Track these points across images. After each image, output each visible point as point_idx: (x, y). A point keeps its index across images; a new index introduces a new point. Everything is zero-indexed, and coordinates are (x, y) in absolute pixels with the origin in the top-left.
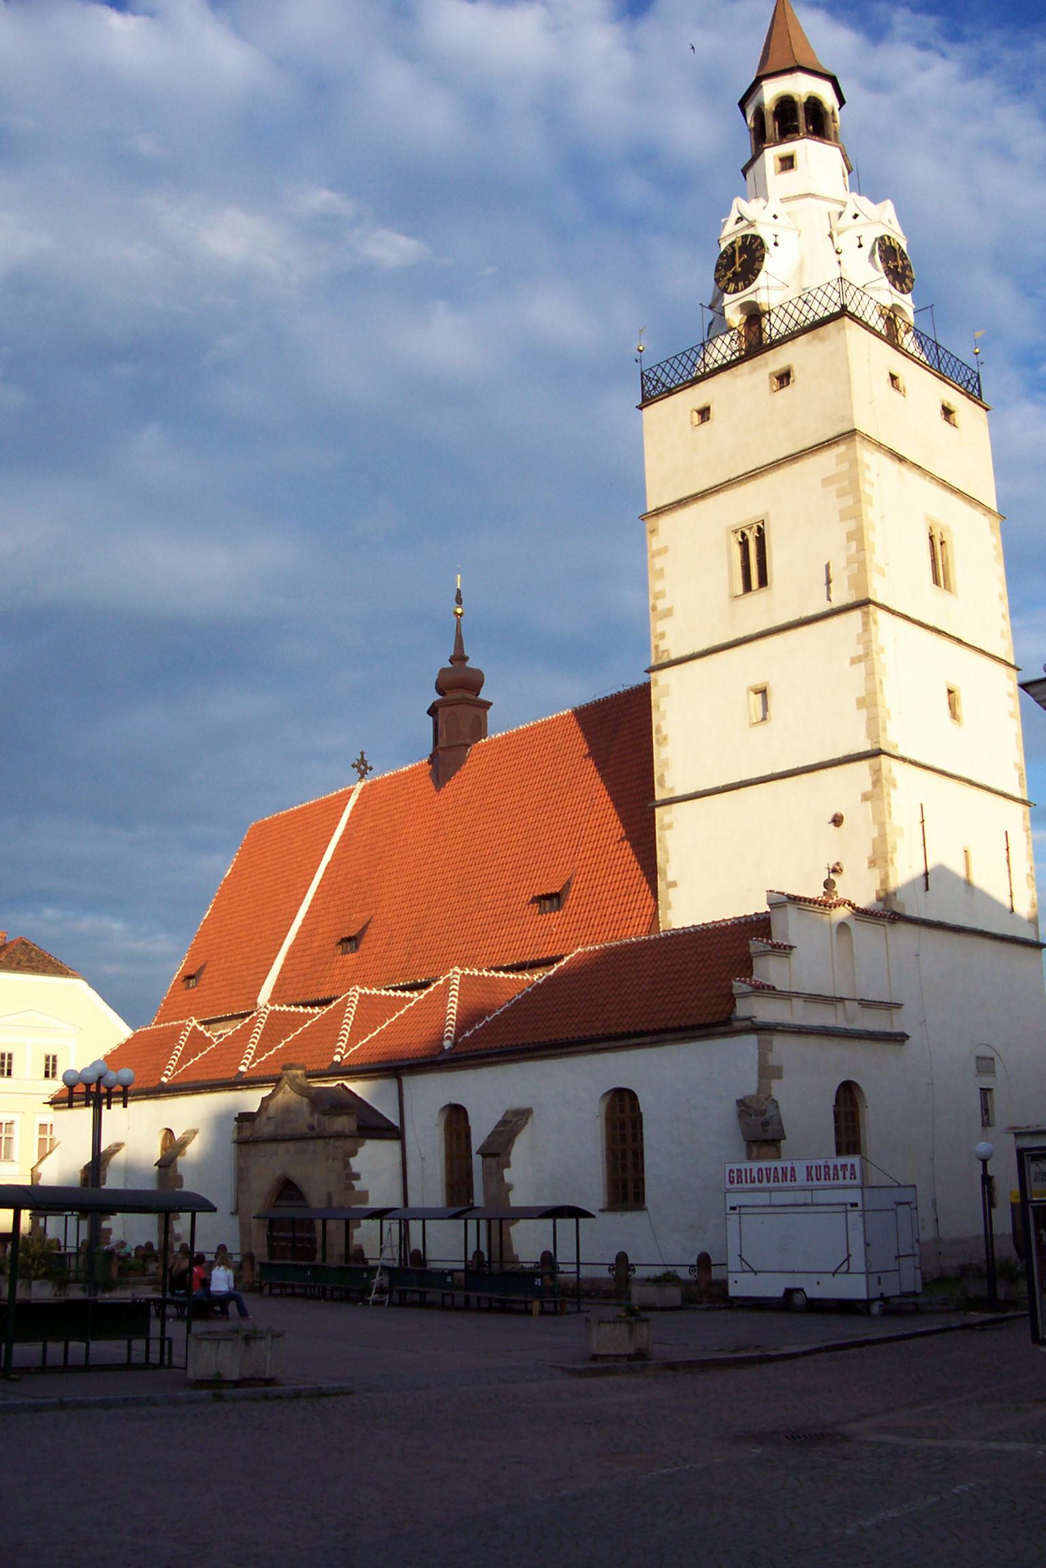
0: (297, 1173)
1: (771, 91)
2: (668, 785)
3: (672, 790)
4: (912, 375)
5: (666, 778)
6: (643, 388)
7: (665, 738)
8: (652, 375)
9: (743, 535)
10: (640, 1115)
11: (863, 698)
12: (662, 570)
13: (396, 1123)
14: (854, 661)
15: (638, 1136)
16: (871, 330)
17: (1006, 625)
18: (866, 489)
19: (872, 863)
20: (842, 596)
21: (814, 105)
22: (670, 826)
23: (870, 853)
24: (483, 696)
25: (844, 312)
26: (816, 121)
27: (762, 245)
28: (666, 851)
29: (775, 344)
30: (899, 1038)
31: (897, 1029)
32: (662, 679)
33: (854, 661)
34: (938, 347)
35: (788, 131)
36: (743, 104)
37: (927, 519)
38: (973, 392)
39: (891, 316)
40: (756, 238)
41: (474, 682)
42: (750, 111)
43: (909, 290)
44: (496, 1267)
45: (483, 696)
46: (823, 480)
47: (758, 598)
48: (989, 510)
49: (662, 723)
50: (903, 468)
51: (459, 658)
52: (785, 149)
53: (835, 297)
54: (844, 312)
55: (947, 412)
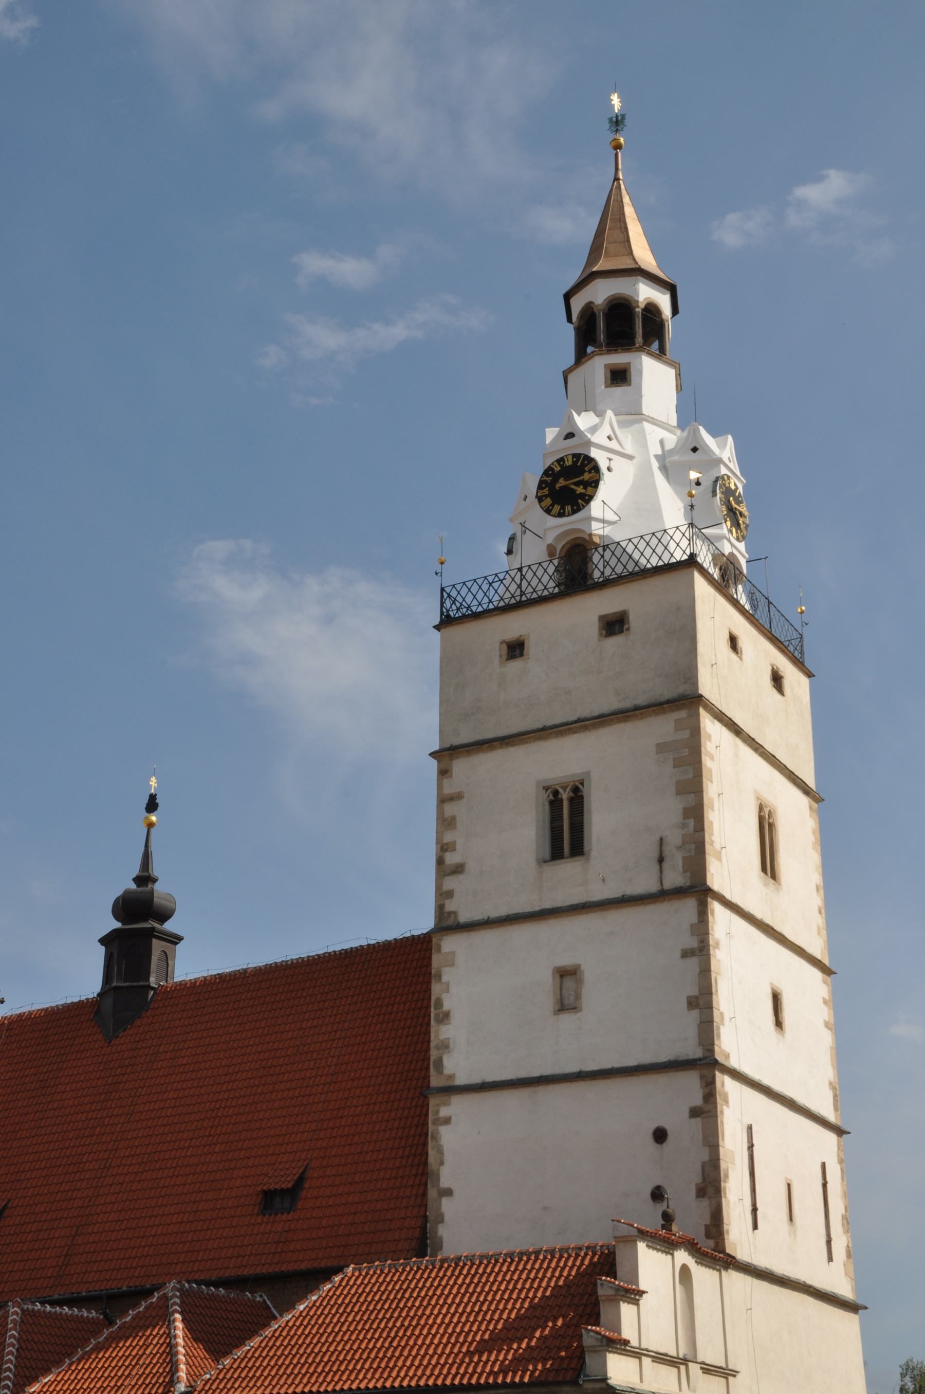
1: (600, 293)
2: (447, 1071)
3: (452, 1077)
4: (748, 635)
6: (442, 606)
7: (447, 1015)
8: (454, 594)
9: (556, 793)
11: (696, 998)
12: (454, 818)
14: (685, 954)
17: (819, 920)
18: (707, 762)
19: (701, 1192)
20: (675, 878)
22: (447, 1121)
23: (698, 1179)
24: (169, 926)
25: (692, 562)
28: (440, 1151)
29: (607, 583)
32: (449, 944)
34: (770, 603)
36: (568, 297)
37: (758, 799)
38: (799, 663)
42: (578, 304)
43: (744, 538)
46: (658, 745)
47: (568, 868)
49: (444, 997)
51: (144, 879)
52: (618, 359)
54: (692, 562)
55: (733, 642)
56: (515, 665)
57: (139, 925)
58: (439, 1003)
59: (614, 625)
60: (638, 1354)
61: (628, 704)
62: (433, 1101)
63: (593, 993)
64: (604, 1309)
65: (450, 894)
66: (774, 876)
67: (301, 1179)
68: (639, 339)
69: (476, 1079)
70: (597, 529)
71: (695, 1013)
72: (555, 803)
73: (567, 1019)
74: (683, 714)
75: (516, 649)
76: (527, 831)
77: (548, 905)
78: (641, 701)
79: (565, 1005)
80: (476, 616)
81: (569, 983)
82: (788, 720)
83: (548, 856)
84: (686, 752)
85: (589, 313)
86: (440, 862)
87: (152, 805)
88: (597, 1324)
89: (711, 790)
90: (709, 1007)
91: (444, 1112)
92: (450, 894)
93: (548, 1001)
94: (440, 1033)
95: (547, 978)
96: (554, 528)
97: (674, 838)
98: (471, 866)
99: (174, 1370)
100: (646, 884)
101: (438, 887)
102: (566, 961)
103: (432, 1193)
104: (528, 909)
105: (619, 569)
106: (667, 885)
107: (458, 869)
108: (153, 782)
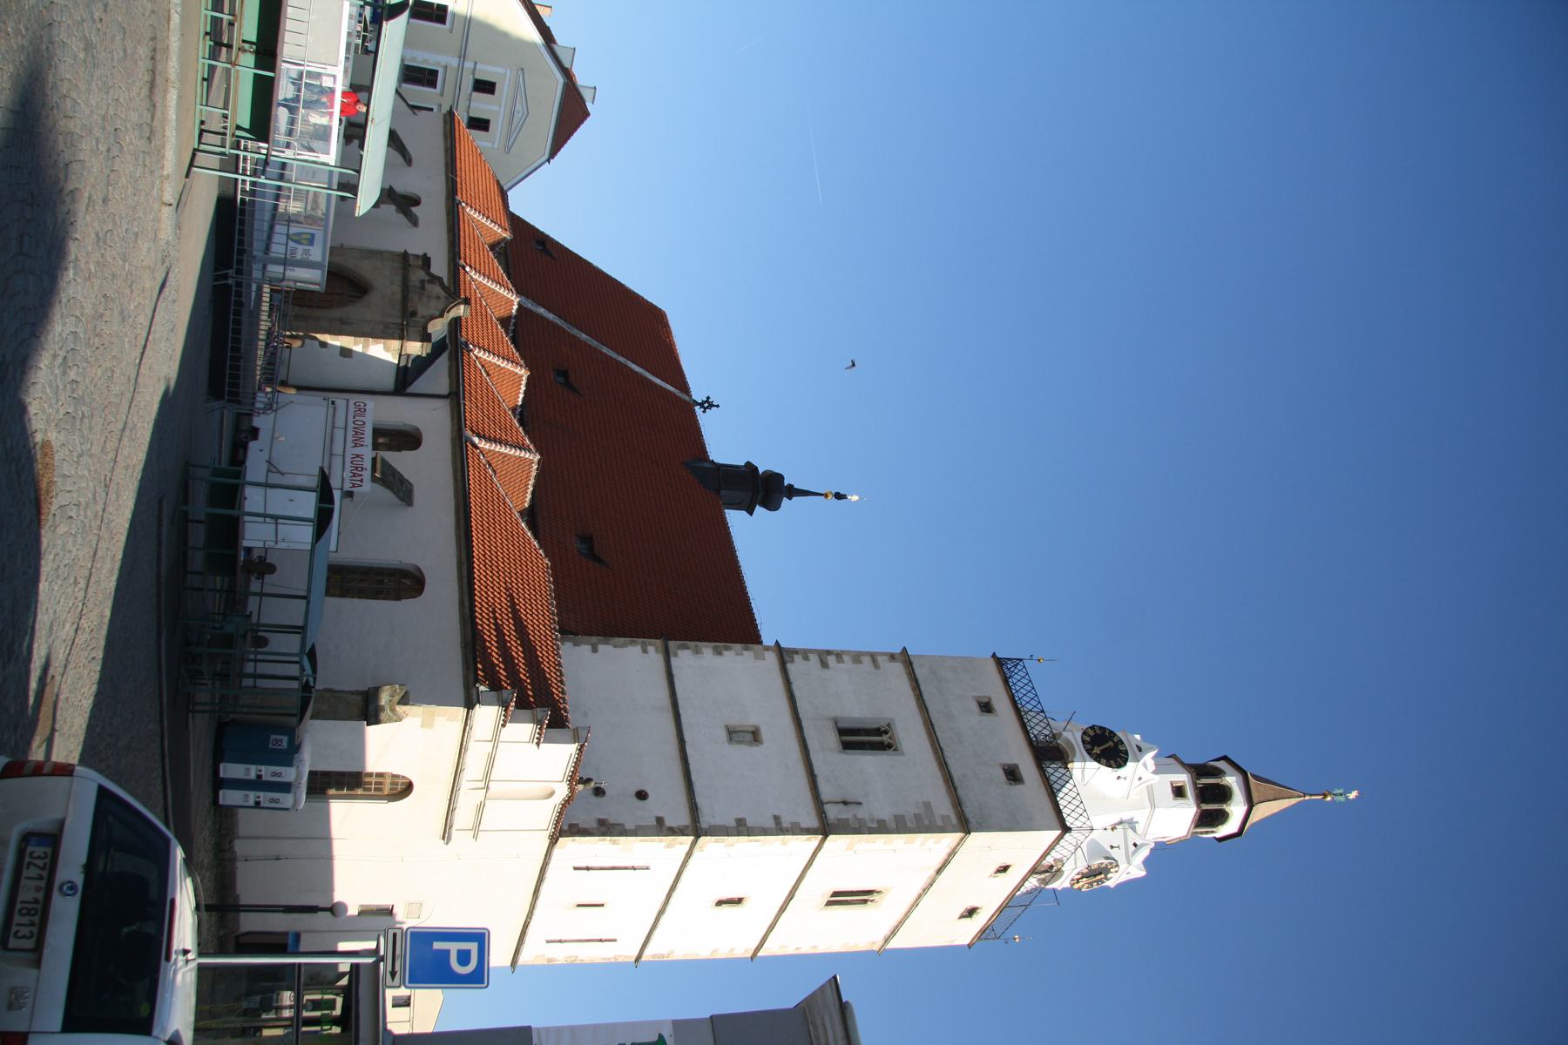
0: (374, 298)
1: (1232, 780)
5: (687, 652)
7: (720, 653)
10: (398, 598)
13: (410, 390)
14: (777, 819)
15: (377, 594)
16: (1047, 853)
19: (602, 822)
20: (833, 812)
21: (1220, 817)
22: (645, 651)
23: (611, 821)
24: (759, 509)
25: (1066, 829)
26: (1209, 819)
27: (1119, 766)
28: (622, 646)
29: (1042, 771)
30: (446, 835)
31: (454, 833)
33: (777, 819)
35: (1204, 795)
36: (1225, 758)
38: (983, 934)
39: (1053, 872)
40: (1125, 762)
41: (772, 505)
42: (1222, 765)
44: (255, 586)
45: (759, 509)
47: (833, 739)
48: (887, 940)
50: (932, 872)
51: (792, 492)
53: (1078, 824)
54: (1066, 829)
56: (975, 707)
57: (764, 489)
58: (728, 649)
59: (1013, 775)
60: (495, 740)
61: (957, 783)
62: (659, 642)
63: (742, 753)
64: (527, 713)
65: (806, 658)
66: (829, 903)
67: (600, 561)
68: (1205, 807)
69: (675, 671)
70: (1076, 767)
71: (733, 824)
72: (878, 732)
73: (723, 734)
74: (954, 820)
75: (986, 707)
76: (858, 711)
77: (804, 724)
78: (961, 792)
79: (733, 734)
80: (1006, 681)
81: (749, 737)
82: (942, 927)
83: (841, 725)
84: (926, 822)
85: (1218, 773)
86: (829, 653)
87: (839, 496)
88: (517, 707)
89: (898, 840)
90: (739, 834)
91: (651, 649)
92: (806, 658)
93: (736, 720)
94: (707, 649)
95: (752, 720)
96: (1073, 737)
97: (862, 813)
98: (826, 673)
99: (489, 439)
100: (826, 791)
101: (811, 651)
102: (765, 734)
103: (594, 639)
104: (800, 711)
105: (1053, 778)
106: (826, 807)
107: (824, 665)
108: (855, 498)
